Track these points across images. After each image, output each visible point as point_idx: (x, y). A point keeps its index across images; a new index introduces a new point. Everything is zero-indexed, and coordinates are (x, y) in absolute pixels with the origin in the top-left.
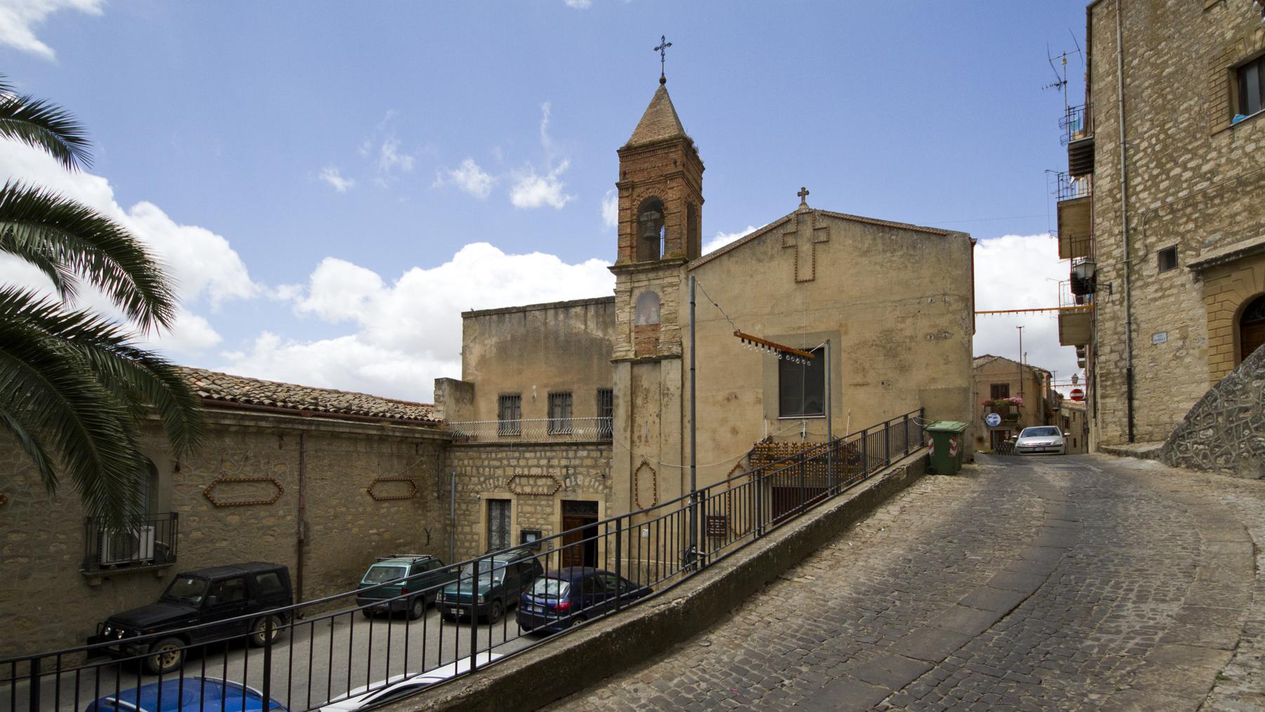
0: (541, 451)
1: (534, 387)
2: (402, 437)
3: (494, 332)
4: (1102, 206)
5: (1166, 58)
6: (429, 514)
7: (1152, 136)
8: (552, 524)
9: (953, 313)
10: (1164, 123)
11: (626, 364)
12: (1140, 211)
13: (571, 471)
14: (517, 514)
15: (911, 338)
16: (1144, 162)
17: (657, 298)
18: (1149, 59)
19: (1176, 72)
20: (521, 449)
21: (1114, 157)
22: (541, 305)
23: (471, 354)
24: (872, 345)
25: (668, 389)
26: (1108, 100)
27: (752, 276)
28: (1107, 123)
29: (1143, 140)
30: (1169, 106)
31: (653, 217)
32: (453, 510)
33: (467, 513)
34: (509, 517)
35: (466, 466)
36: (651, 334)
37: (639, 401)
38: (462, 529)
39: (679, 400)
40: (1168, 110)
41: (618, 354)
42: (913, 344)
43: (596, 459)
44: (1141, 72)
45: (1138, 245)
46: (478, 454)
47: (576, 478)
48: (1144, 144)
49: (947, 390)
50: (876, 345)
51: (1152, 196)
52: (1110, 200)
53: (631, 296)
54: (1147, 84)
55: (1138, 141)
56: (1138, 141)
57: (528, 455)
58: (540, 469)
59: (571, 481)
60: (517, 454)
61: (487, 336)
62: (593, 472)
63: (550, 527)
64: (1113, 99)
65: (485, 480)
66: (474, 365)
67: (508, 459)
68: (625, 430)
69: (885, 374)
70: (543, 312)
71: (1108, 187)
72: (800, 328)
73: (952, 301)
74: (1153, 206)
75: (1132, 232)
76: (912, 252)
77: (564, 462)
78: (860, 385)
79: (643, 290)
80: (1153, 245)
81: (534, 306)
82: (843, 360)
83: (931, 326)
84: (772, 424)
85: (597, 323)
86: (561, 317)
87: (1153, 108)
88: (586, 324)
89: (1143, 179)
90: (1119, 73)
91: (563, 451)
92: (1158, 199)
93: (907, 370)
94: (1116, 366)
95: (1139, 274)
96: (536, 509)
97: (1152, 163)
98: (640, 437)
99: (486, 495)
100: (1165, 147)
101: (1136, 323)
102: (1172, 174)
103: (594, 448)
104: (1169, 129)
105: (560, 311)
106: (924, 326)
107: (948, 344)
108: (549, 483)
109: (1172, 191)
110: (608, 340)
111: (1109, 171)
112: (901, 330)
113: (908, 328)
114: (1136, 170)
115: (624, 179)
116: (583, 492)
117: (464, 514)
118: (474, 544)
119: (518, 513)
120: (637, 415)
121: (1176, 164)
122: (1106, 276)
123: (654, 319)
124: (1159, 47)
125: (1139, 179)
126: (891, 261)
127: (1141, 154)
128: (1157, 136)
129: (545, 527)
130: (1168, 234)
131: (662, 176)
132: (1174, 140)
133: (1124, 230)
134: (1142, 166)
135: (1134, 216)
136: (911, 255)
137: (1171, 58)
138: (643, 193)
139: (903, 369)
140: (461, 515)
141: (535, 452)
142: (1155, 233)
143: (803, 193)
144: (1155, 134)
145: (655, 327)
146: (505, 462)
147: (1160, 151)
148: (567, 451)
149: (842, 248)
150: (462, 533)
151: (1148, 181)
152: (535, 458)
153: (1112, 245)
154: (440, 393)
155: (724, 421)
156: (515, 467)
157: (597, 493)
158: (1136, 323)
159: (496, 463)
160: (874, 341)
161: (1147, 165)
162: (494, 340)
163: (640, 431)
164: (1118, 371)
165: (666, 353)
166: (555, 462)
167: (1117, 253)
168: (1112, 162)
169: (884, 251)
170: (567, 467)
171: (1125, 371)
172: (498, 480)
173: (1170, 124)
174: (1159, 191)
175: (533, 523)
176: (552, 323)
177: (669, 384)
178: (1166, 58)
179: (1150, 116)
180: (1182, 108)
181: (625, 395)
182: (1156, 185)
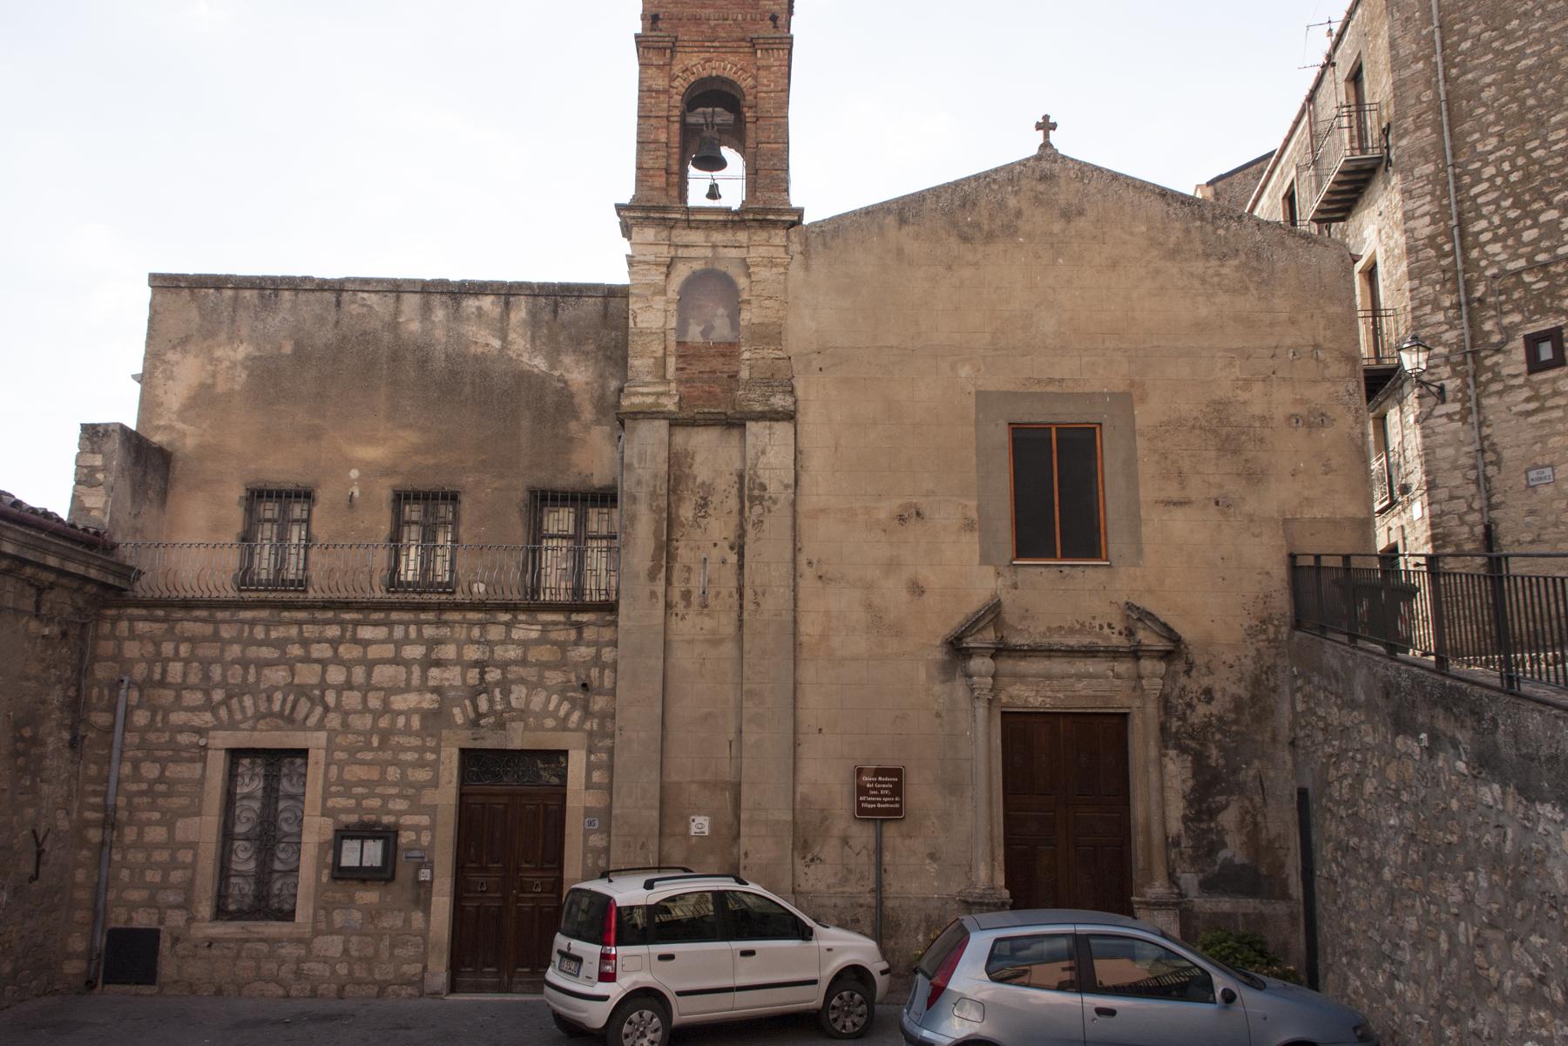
0: (407, 624)
2: (14, 558)
3: (244, 332)
4: (1417, 261)
5: (1520, 43)
6: (46, 788)
7: (1502, 159)
8: (432, 810)
9: (1333, 380)
10: (1525, 140)
11: (657, 423)
12: (1488, 273)
13: (493, 675)
14: (326, 789)
15: (1263, 418)
16: (1492, 196)
17: (728, 283)
18: (1491, 42)
19: (1541, 66)
20: (348, 616)
21: (1434, 186)
22: (388, 281)
24: (1193, 427)
25: (763, 487)
26: (1418, 98)
27: (950, 268)
28: (1418, 134)
29: (1486, 164)
30: (1531, 116)
31: (718, 120)
32: (113, 780)
33: (162, 788)
34: (298, 798)
35: (167, 660)
36: (718, 364)
37: (686, 512)
38: (140, 834)
39: (788, 512)
40: (1530, 120)
41: (636, 400)
42: (1267, 432)
43: (562, 646)
44: (1476, 62)
45: (1488, 326)
46: (208, 629)
47: (506, 693)
48: (1489, 171)
49: (1331, 522)
50: (1201, 428)
51: (1509, 251)
52: (1432, 253)
53: (668, 275)
54: (1488, 79)
55: (1477, 165)
56: (1477, 165)
57: (366, 633)
58: (402, 670)
59: (491, 701)
60: (333, 631)
61: (223, 337)
62: (554, 678)
63: (424, 820)
64: (1427, 96)
65: (229, 697)
67: (305, 643)
68: (652, 576)
69: (1221, 486)
70: (391, 298)
71: (1427, 231)
72: (1051, 381)
73: (1329, 360)
74: (1511, 266)
75: (1476, 305)
76: (1255, 264)
77: (472, 653)
78: (1175, 504)
79: (698, 266)
80: (1515, 327)
81: (366, 281)
82: (1139, 453)
83: (1295, 402)
84: (998, 574)
85: (533, 338)
86: (439, 314)
87: (1500, 116)
88: (504, 339)
89: (1490, 223)
90: (1438, 58)
91: (472, 624)
92: (1521, 256)
93: (1260, 480)
94: (1462, 522)
95: (1493, 372)
96: (383, 773)
97: (1505, 200)
98: (686, 595)
99: (224, 739)
100: (1527, 177)
101: (1495, 451)
102: (1543, 218)
103: (559, 617)
104: (1534, 149)
105: (436, 300)
106: (1282, 400)
107: (1326, 435)
108: (425, 705)
109: (1545, 244)
110: (561, 379)
111: (1427, 208)
112: (1244, 403)
113: (1255, 401)
114: (1478, 208)
115: (652, 30)
116: (526, 728)
117: (150, 792)
118: (176, 876)
119: (327, 783)
120: (681, 544)
121: (1550, 205)
122: (1433, 374)
123: (722, 331)
124: (1508, 27)
125: (1483, 224)
126: (1219, 275)
127: (1485, 186)
128: (1512, 159)
129: (407, 820)
130: (1543, 311)
131: (743, 40)
132: (1542, 167)
133: (1463, 299)
134: (1487, 204)
135: (1479, 280)
136: (1254, 269)
137: (1530, 44)
138: (695, 64)
139: (1254, 476)
140: (142, 793)
141: (390, 624)
142: (1518, 308)
143: (1046, 126)
144: (1508, 156)
145: (729, 350)
146: (296, 650)
147: (1519, 182)
148: (483, 625)
149: (1127, 237)
150: (139, 844)
151: (1499, 227)
152: (388, 640)
153: (1440, 323)
154: (98, 461)
155: (892, 566)
157: (565, 729)
158: (1495, 451)
159: (266, 653)
160: (1195, 419)
161: (1496, 202)
162: (242, 351)
163: (688, 580)
164: (1466, 529)
165: (758, 407)
166: (449, 652)
167: (1450, 336)
168: (1432, 194)
169: (1207, 256)
170: (481, 665)
171: (1479, 530)
172: (270, 699)
173: (1536, 143)
174: (1520, 243)
175: (370, 810)
176: (415, 326)
177: (765, 476)
178: (1520, 43)
179: (1497, 129)
180: (1553, 120)
181: (653, 495)
182: (1517, 235)
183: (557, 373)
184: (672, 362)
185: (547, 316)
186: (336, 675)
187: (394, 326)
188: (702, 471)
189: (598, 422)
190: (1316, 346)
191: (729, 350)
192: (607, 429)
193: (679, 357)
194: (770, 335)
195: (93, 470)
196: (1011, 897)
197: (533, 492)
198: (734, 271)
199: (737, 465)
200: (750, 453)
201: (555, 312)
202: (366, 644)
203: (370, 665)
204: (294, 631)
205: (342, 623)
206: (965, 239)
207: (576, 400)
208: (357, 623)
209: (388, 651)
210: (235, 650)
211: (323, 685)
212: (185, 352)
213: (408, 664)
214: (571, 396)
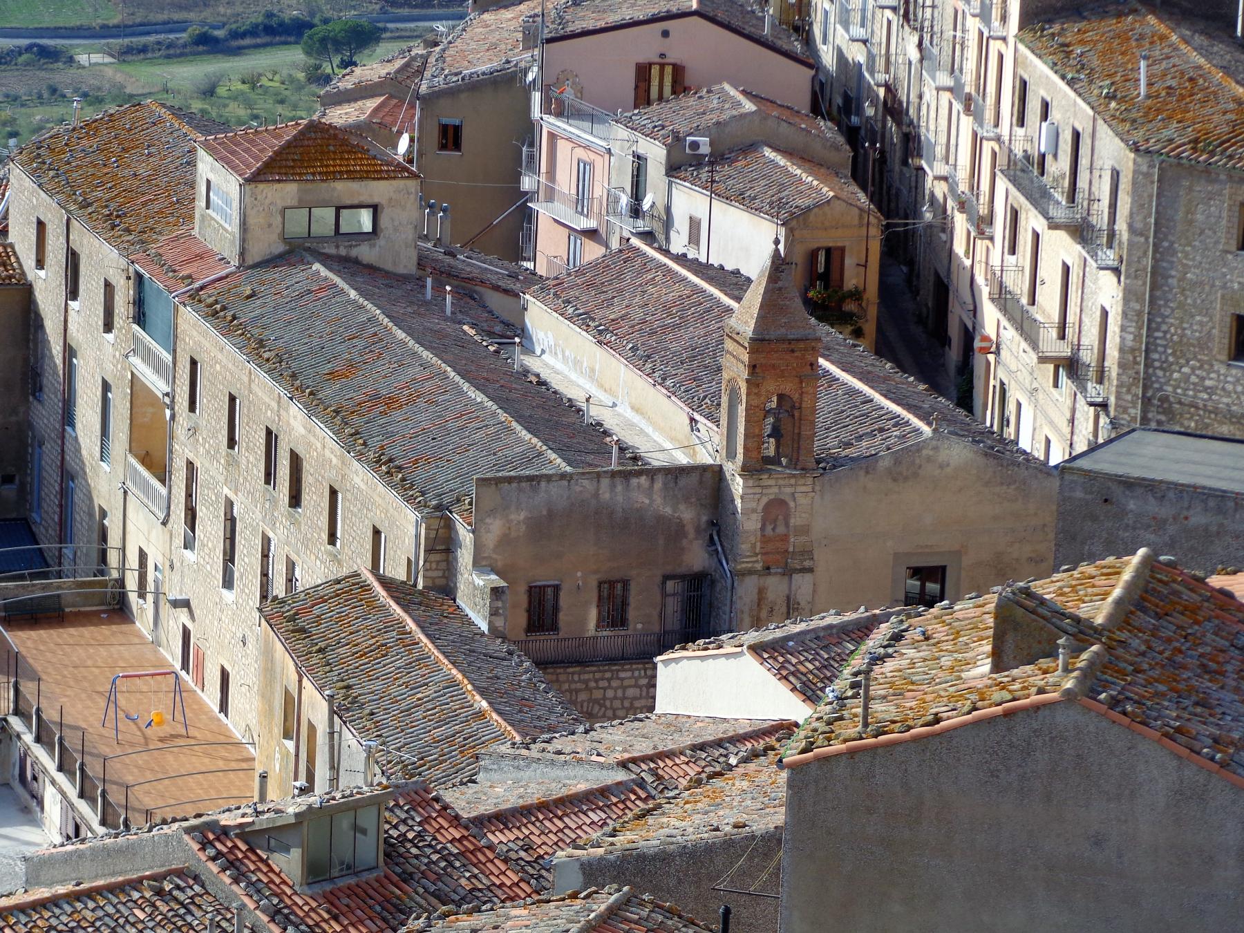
1: (579, 574)
15: (1017, 560)
23: (488, 531)
41: (744, 565)
46: (554, 677)
57: (622, 675)
60: (608, 675)
66: (491, 546)
67: (596, 681)
79: (772, 497)
85: (665, 497)
86: (619, 488)
105: (618, 480)
123: (781, 529)
141: (632, 671)
146: (593, 684)
152: (632, 677)
154: (500, 604)
156: (605, 689)
169: (1002, 484)
176: (607, 496)
181: (751, 610)
183: (676, 515)
184: (758, 544)
185: (672, 485)
186: (610, 693)
187: (596, 495)
188: (770, 596)
189: (696, 539)
190: (1044, 525)
191: (785, 538)
192: (701, 542)
193: (761, 542)
194: (805, 530)
195: (498, 608)
196: (520, 174)
197: (664, 576)
198: (788, 499)
199: (787, 592)
200: (793, 588)
201: (676, 483)
202: (622, 679)
203: (624, 688)
204: (591, 675)
205: (612, 671)
206: (895, 480)
207: (686, 528)
208: (618, 671)
209: (632, 682)
210: (566, 686)
211: (604, 698)
212: (495, 518)
213: (640, 687)
214: (683, 526)
